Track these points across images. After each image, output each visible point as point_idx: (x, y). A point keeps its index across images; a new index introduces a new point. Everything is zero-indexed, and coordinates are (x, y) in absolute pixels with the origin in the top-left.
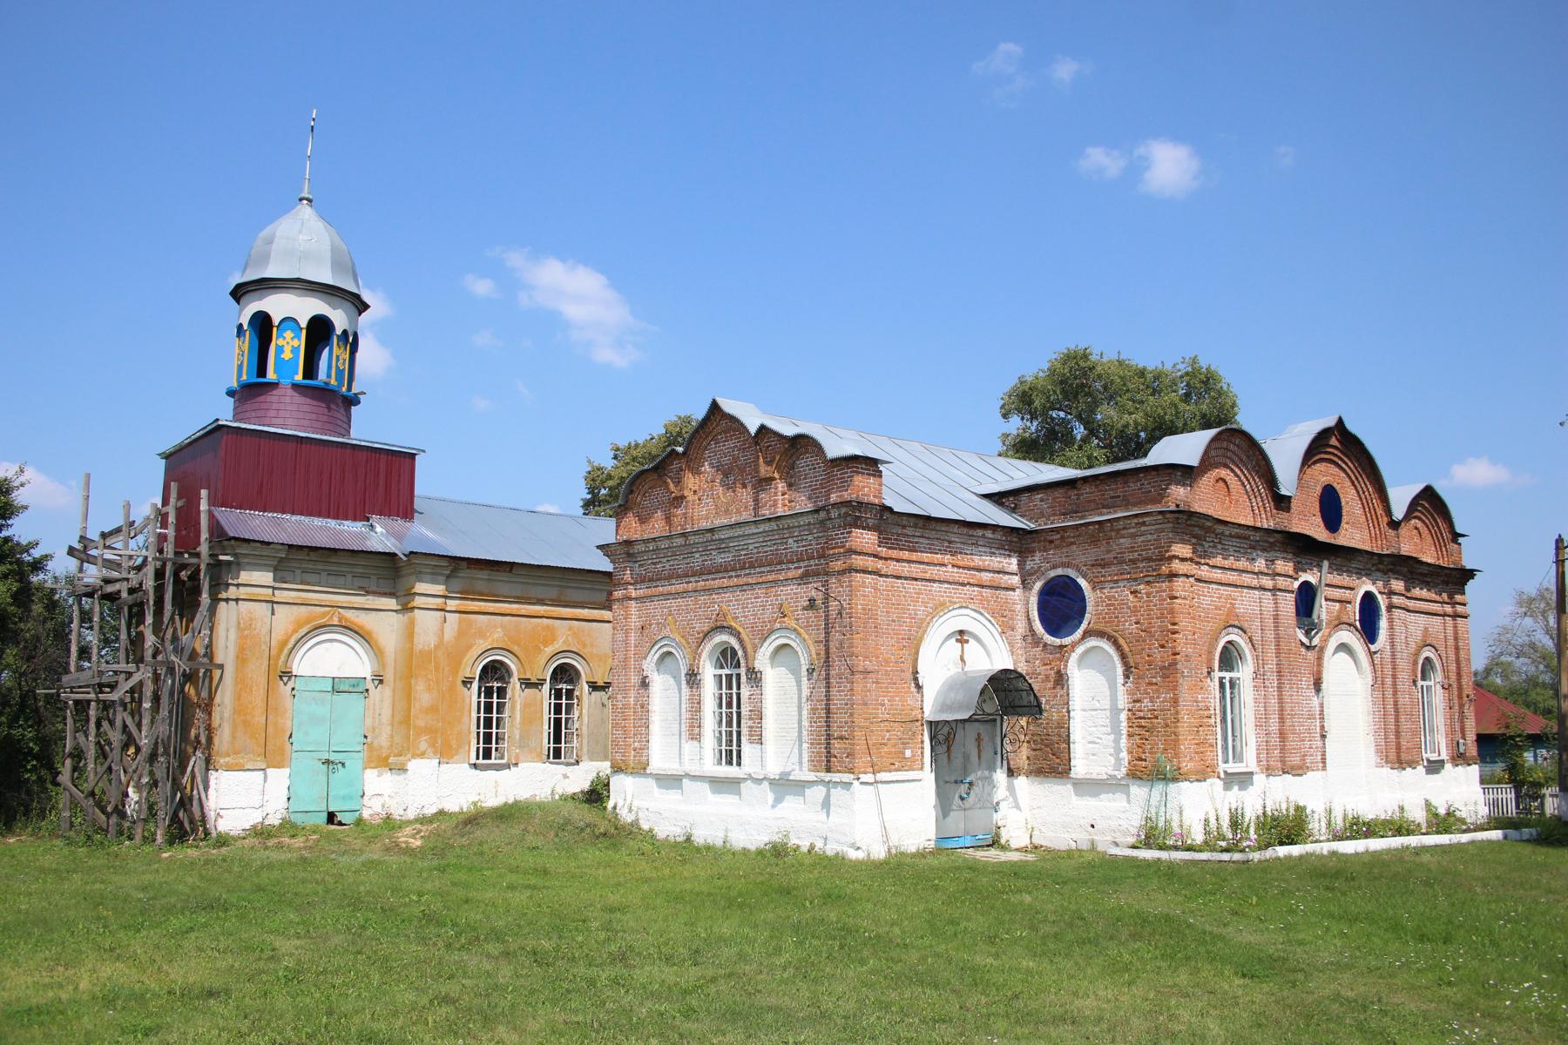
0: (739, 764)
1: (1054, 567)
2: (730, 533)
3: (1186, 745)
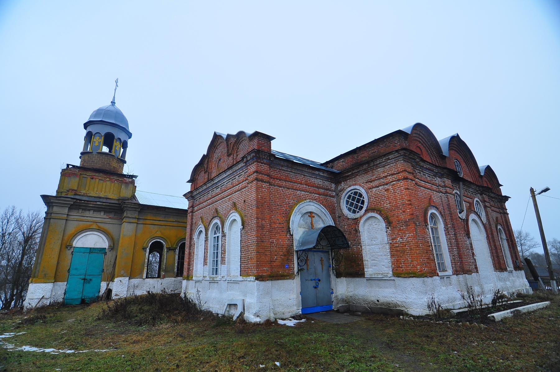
0: (216, 274)
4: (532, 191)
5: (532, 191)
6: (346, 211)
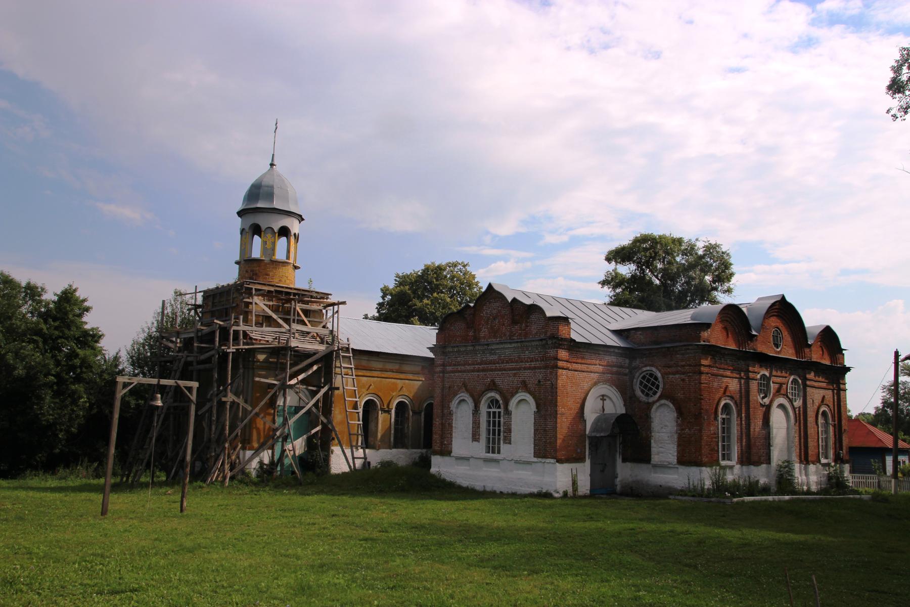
1: (646, 366)
2: (498, 346)
3: (705, 450)
4: (897, 354)
5: (897, 354)
6: (638, 393)
